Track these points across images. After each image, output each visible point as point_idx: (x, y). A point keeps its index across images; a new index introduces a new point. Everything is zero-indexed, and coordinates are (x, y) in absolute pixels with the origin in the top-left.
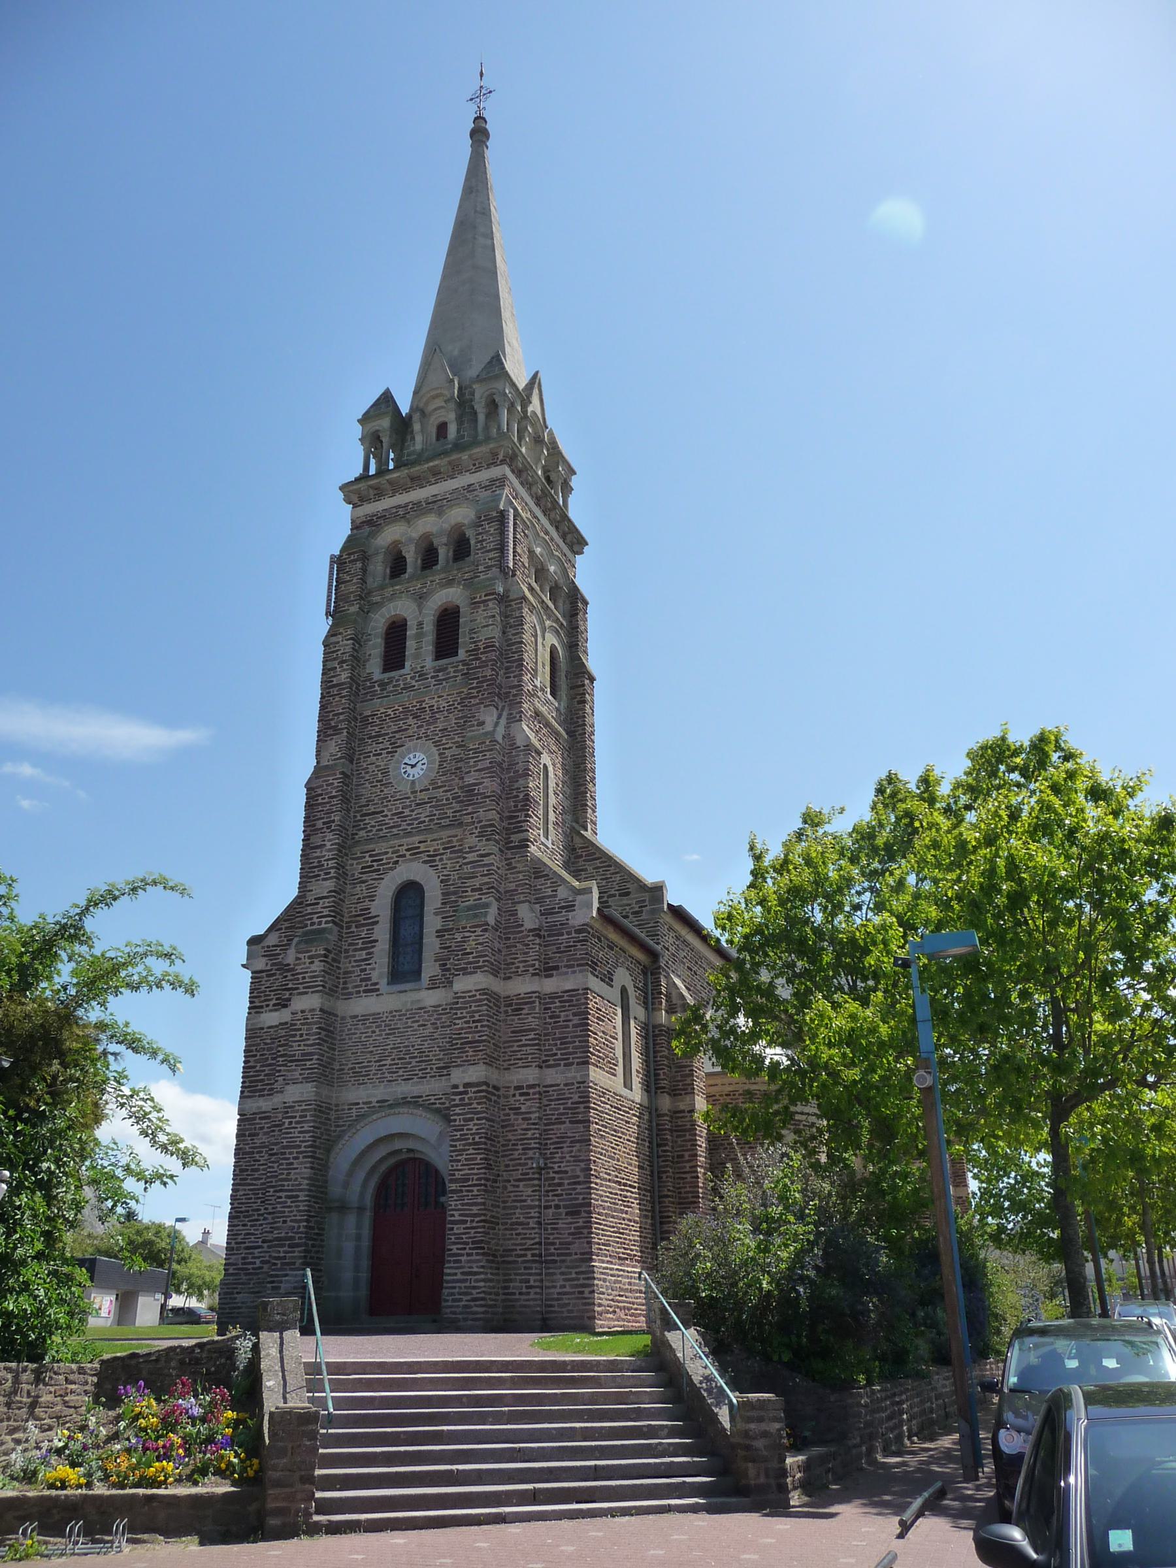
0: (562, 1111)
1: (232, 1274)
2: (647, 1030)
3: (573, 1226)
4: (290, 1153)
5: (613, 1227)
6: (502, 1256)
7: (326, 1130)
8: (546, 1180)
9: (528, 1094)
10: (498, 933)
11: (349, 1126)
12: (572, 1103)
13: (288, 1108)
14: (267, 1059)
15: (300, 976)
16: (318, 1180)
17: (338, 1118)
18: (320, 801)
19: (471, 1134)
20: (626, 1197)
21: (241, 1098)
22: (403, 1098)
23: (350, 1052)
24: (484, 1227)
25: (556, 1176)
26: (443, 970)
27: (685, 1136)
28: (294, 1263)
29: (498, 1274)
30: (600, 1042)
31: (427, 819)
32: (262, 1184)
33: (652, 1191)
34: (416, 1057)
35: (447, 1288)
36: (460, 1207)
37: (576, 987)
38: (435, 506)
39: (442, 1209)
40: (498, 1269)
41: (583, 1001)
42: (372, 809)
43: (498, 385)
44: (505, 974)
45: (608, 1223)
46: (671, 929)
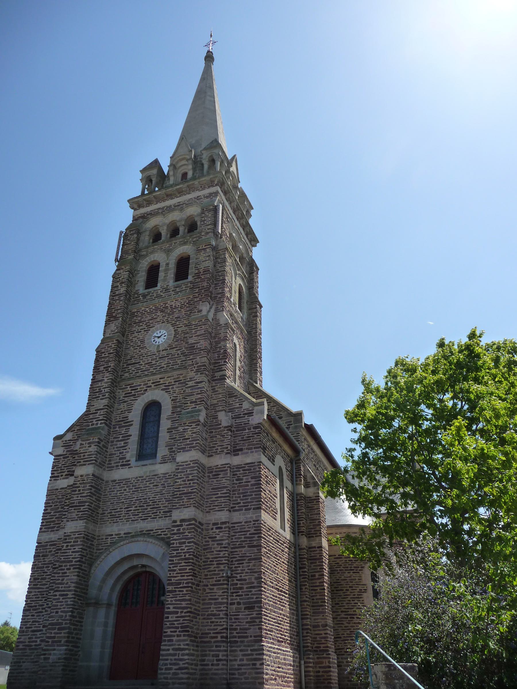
0: (243, 539)
1: (21, 649)
2: (293, 497)
3: (249, 617)
4: (65, 566)
5: (275, 619)
6: (201, 638)
7: (89, 551)
8: (232, 585)
9: (221, 528)
10: (206, 428)
11: (105, 549)
12: (250, 534)
13: (67, 536)
14: (58, 508)
15: (82, 455)
16: (82, 585)
17: (99, 545)
18: (103, 356)
19: (184, 553)
20: (282, 599)
21: (40, 532)
22: (140, 532)
23: (110, 502)
24: (189, 616)
25: (239, 582)
26: (171, 452)
27: (316, 563)
28: (60, 641)
29: (197, 651)
30: (268, 497)
31: (165, 366)
32: (47, 588)
33: (296, 597)
34: (151, 505)
35: (162, 660)
36: (174, 602)
37: (253, 461)
38: (180, 207)
39: (162, 604)
40: (197, 646)
41: (258, 469)
42: (133, 361)
43: (216, 151)
44: (209, 453)
45: (272, 616)
46: (305, 439)
